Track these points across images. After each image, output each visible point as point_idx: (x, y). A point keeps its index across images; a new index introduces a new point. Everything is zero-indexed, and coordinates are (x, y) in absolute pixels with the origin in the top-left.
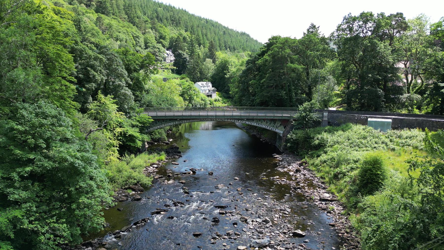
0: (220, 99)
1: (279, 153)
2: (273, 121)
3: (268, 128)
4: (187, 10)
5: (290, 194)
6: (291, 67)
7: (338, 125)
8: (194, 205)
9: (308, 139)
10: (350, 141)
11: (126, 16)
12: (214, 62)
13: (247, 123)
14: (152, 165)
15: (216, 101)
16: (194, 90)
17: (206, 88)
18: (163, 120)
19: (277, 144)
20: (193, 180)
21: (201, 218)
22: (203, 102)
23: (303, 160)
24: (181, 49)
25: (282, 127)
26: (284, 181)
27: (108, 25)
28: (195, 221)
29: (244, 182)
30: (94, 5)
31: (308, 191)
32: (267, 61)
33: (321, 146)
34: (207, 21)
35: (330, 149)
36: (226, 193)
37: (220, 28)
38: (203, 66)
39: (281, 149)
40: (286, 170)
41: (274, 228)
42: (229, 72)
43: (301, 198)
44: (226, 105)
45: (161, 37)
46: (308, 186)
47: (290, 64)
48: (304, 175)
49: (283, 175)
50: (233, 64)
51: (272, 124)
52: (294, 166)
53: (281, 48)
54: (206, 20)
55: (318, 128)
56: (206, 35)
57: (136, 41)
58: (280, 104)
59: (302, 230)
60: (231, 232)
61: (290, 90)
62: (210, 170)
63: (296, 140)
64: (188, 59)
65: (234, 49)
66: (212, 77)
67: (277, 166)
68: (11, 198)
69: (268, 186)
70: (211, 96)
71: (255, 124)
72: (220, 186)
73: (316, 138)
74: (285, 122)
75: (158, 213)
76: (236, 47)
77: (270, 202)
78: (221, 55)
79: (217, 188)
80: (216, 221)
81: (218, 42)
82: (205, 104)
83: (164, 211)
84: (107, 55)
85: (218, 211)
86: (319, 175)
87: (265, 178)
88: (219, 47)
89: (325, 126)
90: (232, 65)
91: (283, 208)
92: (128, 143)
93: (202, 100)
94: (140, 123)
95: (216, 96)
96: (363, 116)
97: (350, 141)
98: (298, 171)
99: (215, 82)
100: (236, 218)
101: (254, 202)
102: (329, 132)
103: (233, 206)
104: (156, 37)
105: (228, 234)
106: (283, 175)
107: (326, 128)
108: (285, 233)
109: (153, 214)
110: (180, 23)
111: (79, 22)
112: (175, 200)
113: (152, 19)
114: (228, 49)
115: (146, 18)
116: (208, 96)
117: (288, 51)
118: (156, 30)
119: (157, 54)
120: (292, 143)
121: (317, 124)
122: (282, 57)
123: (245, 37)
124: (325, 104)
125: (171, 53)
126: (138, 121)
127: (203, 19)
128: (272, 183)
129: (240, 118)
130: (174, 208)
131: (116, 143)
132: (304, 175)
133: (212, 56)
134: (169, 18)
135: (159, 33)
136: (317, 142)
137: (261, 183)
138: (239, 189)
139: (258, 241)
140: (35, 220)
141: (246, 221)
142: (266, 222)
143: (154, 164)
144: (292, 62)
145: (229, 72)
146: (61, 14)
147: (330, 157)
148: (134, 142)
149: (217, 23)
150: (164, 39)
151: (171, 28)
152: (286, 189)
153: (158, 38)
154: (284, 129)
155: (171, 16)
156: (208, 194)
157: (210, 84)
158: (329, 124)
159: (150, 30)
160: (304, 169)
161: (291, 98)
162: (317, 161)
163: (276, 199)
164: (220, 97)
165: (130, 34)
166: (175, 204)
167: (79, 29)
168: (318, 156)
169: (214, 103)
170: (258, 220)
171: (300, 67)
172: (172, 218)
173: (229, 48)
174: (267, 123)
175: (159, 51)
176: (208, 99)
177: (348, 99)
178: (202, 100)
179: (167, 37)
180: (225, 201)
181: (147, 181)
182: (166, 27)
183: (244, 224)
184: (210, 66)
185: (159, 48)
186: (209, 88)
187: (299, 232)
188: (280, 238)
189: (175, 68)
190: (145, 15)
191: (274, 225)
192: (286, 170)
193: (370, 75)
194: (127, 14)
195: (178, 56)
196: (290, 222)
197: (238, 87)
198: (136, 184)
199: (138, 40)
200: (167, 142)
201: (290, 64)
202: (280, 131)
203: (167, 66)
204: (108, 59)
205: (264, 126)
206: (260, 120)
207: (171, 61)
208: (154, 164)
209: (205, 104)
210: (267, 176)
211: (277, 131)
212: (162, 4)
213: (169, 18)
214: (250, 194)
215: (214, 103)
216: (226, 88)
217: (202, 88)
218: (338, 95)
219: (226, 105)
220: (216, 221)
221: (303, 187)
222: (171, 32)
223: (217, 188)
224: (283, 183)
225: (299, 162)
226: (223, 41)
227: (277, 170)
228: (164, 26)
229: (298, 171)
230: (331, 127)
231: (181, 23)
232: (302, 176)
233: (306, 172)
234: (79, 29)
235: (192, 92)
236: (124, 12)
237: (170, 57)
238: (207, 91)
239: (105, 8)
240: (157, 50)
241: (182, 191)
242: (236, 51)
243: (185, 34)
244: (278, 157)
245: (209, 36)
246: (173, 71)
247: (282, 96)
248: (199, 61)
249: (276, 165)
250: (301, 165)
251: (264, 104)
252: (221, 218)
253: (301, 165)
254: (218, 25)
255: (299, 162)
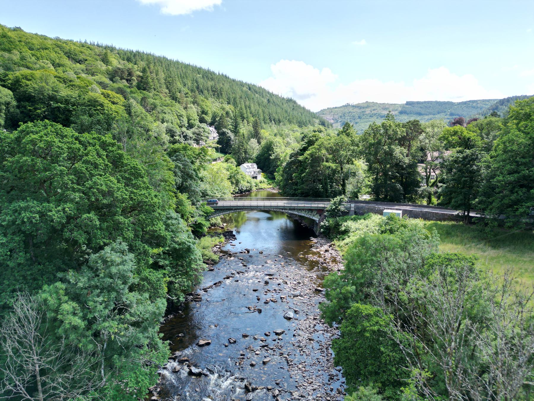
0: (265, 180)
1: (315, 237)
2: (311, 210)
3: (307, 216)
4: (228, 75)
5: (318, 267)
6: (326, 166)
7: (362, 214)
8: (251, 274)
9: (337, 225)
10: (368, 228)
11: (167, 91)
12: (259, 143)
13: (289, 211)
14: (215, 246)
15: (261, 182)
16: (241, 175)
17: (252, 170)
18: (221, 210)
19: (315, 229)
20: (247, 258)
21: (256, 281)
22: (249, 185)
23: (333, 243)
24: (225, 127)
25: (318, 215)
26: (315, 258)
27: (152, 104)
28: (253, 283)
29: (285, 259)
30: (134, 80)
31: (331, 265)
32: (307, 158)
33: (346, 232)
34: (250, 87)
35: (352, 234)
36: (273, 266)
37: (264, 94)
38: (248, 147)
39: (317, 234)
40: (318, 250)
41: (304, 286)
42: (274, 153)
43: (325, 269)
44: (271, 186)
45: (203, 112)
46: (332, 261)
47: (325, 163)
48: (331, 254)
49: (314, 253)
50: (278, 144)
51: (310, 213)
52: (326, 247)
53: (318, 149)
54: (249, 85)
55: (346, 217)
56: (250, 107)
57: (180, 120)
58: (317, 196)
59: (321, 288)
60: (276, 288)
61: (326, 183)
62: (260, 250)
63: (328, 226)
64: (232, 137)
65: (280, 121)
66: (257, 158)
67: (312, 247)
68: (161, 264)
69: (303, 261)
70: (256, 177)
71: (296, 213)
72: (269, 262)
73: (343, 225)
74: (320, 211)
75: (228, 278)
76: (281, 119)
77: (303, 271)
78: (267, 133)
79: (266, 263)
80: (267, 283)
81: (262, 114)
82: (251, 187)
83: (232, 277)
84: (183, 161)
85: (268, 277)
86: (341, 254)
87: (302, 256)
88: (264, 120)
89: (352, 215)
90: (277, 146)
91: (311, 275)
92: (198, 229)
93: (248, 182)
94: (205, 213)
95: (261, 177)
96: (381, 207)
97: (368, 228)
98: (327, 251)
99: (260, 162)
100: (280, 281)
101: (292, 272)
102: (354, 220)
103: (278, 274)
104: (198, 112)
105: (275, 290)
106: (314, 253)
107: (353, 217)
108: (310, 289)
109: (224, 279)
110: (221, 94)
111: (129, 107)
112: (238, 271)
113: (192, 91)
114: (273, 121)
115: (185, 90)
116: (253, 178)
117: (324, 151)
118: (198, 105)
119: (202, 134)
120: (325, 229)
121: (345, 214)
122: (318, 157)
123: (291, 104)
124: (355, 195)
125: (214, 129)
126: (203, 212)
127: (246, 84)
128: (306, 260)
129: (284, 208)
130: (237, 275)
131: (190, 229)
132: (331, 254)
133: (256, 135)
134: (210, 88)
135: (202, 108)
136: (343, 228)
137: (298, 260)
138: (283, 263)
139: (293, 293)
140: (172, 276)
141: (286, 283)
142: (299, 283)
143: (216, 245)
144: (327, 161)
145: (274, 153)
146: (111, 98)
147: (351, 240)
148: (201, 228)
149: (260, 88)
150: (206, 114)
151: (213, 100)
152: (316, 263)
153: (200, 113)
154: (319, 217)
155: (212, 87)
156: (260, 266)
157: (255, 166)
158: (356, 213)
159: (192, 105)
160: (332, 249)
161: (327, 190)
162: (342, 243)
163: (308, 270)
164: (265, 178)
165: (174, 113)
166: (238, 273)
167: (129, 113)
168: (343, 240)
169: (260, 184)
170: (294, 282)
171: (333, 166)
172: (238, 281)
173: (274, 120)
174: (305, 212)
175: (204, 131)
176: (253, 181)
177: (376, 190)
178: (248, 182)
179: (209, 112)
180: (272, 271)
181: (215, 257)
182: (207, 99)
183: (285, 285)
184: (254, 148)
185: (203, 128)
186: (254, 169)
187: (320, 288)
188: (307, 292)
189: (218, 145)
190: (185, 86)
191: (304, 285)
192: (318, 250)
193: (390, 173)
194: (168, 88)
195: (222, 134)
196: (315, 283)
197: (282, 176)
198: (208, 260)
199: (182, 118)
200: (222, 226)
201: (325, 163)
202: (316, 218)
203: (211, 144)
204: (183, 165)
205: (303, 214)
206: (300, 210)
207: (214, 138)
208: (216, 245)
209: (251, 187)
210: (303, 254)
211: (314, 218)
212: (200, 68)
213: (210, 88)
214: (290, 267)
215: (260, 184)
216: (271, 169)
217: (248, 170)
218: (366, 186)
219: (271, 186)
220: (267, 283)
221: (328, 262)
222: (213, 106)
223: (266, 263)
224: (314, 260)
225: (329, 244)
226: (267, 113)
227: (311, 250)
228: (205, 100)
229: (327, 251)
230: (357, 216)
231: (224, 96)
232: (330, 255)
233: (333, 252)
234: (129, 113)
235: (239, 177)
236: (165, 86)
237: (213, 135)
238: (253, 173)
239: (147, 83)
240: (201, 130)
241: (241, 265)
242: (281, 124)
243: (228, 107)
244: (314, 240)
245: (252, 108)
246: (217, 149)
247: (319, 189)
248: (244, 142)
249: (311, 247)
250: (330, 246)
251: (305, 196)
252: (270, 281)
253: (330, 246)
254: (261, 91)
255: (329, 244)
